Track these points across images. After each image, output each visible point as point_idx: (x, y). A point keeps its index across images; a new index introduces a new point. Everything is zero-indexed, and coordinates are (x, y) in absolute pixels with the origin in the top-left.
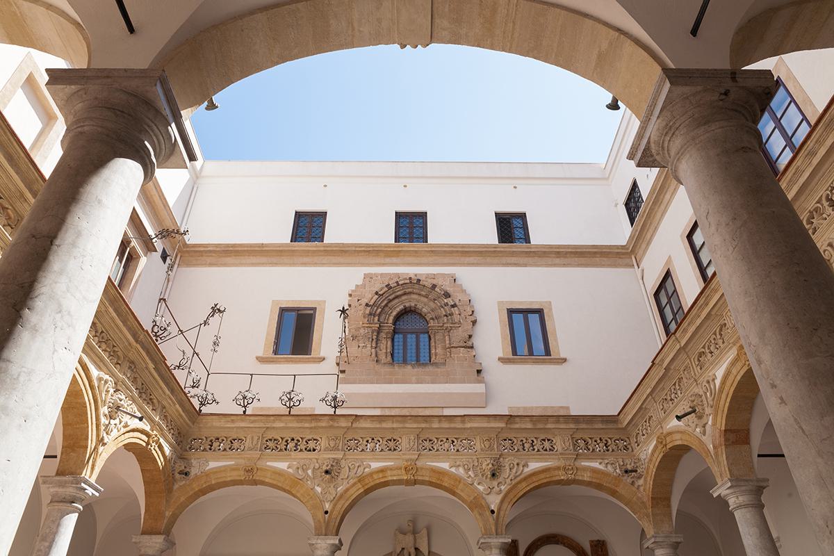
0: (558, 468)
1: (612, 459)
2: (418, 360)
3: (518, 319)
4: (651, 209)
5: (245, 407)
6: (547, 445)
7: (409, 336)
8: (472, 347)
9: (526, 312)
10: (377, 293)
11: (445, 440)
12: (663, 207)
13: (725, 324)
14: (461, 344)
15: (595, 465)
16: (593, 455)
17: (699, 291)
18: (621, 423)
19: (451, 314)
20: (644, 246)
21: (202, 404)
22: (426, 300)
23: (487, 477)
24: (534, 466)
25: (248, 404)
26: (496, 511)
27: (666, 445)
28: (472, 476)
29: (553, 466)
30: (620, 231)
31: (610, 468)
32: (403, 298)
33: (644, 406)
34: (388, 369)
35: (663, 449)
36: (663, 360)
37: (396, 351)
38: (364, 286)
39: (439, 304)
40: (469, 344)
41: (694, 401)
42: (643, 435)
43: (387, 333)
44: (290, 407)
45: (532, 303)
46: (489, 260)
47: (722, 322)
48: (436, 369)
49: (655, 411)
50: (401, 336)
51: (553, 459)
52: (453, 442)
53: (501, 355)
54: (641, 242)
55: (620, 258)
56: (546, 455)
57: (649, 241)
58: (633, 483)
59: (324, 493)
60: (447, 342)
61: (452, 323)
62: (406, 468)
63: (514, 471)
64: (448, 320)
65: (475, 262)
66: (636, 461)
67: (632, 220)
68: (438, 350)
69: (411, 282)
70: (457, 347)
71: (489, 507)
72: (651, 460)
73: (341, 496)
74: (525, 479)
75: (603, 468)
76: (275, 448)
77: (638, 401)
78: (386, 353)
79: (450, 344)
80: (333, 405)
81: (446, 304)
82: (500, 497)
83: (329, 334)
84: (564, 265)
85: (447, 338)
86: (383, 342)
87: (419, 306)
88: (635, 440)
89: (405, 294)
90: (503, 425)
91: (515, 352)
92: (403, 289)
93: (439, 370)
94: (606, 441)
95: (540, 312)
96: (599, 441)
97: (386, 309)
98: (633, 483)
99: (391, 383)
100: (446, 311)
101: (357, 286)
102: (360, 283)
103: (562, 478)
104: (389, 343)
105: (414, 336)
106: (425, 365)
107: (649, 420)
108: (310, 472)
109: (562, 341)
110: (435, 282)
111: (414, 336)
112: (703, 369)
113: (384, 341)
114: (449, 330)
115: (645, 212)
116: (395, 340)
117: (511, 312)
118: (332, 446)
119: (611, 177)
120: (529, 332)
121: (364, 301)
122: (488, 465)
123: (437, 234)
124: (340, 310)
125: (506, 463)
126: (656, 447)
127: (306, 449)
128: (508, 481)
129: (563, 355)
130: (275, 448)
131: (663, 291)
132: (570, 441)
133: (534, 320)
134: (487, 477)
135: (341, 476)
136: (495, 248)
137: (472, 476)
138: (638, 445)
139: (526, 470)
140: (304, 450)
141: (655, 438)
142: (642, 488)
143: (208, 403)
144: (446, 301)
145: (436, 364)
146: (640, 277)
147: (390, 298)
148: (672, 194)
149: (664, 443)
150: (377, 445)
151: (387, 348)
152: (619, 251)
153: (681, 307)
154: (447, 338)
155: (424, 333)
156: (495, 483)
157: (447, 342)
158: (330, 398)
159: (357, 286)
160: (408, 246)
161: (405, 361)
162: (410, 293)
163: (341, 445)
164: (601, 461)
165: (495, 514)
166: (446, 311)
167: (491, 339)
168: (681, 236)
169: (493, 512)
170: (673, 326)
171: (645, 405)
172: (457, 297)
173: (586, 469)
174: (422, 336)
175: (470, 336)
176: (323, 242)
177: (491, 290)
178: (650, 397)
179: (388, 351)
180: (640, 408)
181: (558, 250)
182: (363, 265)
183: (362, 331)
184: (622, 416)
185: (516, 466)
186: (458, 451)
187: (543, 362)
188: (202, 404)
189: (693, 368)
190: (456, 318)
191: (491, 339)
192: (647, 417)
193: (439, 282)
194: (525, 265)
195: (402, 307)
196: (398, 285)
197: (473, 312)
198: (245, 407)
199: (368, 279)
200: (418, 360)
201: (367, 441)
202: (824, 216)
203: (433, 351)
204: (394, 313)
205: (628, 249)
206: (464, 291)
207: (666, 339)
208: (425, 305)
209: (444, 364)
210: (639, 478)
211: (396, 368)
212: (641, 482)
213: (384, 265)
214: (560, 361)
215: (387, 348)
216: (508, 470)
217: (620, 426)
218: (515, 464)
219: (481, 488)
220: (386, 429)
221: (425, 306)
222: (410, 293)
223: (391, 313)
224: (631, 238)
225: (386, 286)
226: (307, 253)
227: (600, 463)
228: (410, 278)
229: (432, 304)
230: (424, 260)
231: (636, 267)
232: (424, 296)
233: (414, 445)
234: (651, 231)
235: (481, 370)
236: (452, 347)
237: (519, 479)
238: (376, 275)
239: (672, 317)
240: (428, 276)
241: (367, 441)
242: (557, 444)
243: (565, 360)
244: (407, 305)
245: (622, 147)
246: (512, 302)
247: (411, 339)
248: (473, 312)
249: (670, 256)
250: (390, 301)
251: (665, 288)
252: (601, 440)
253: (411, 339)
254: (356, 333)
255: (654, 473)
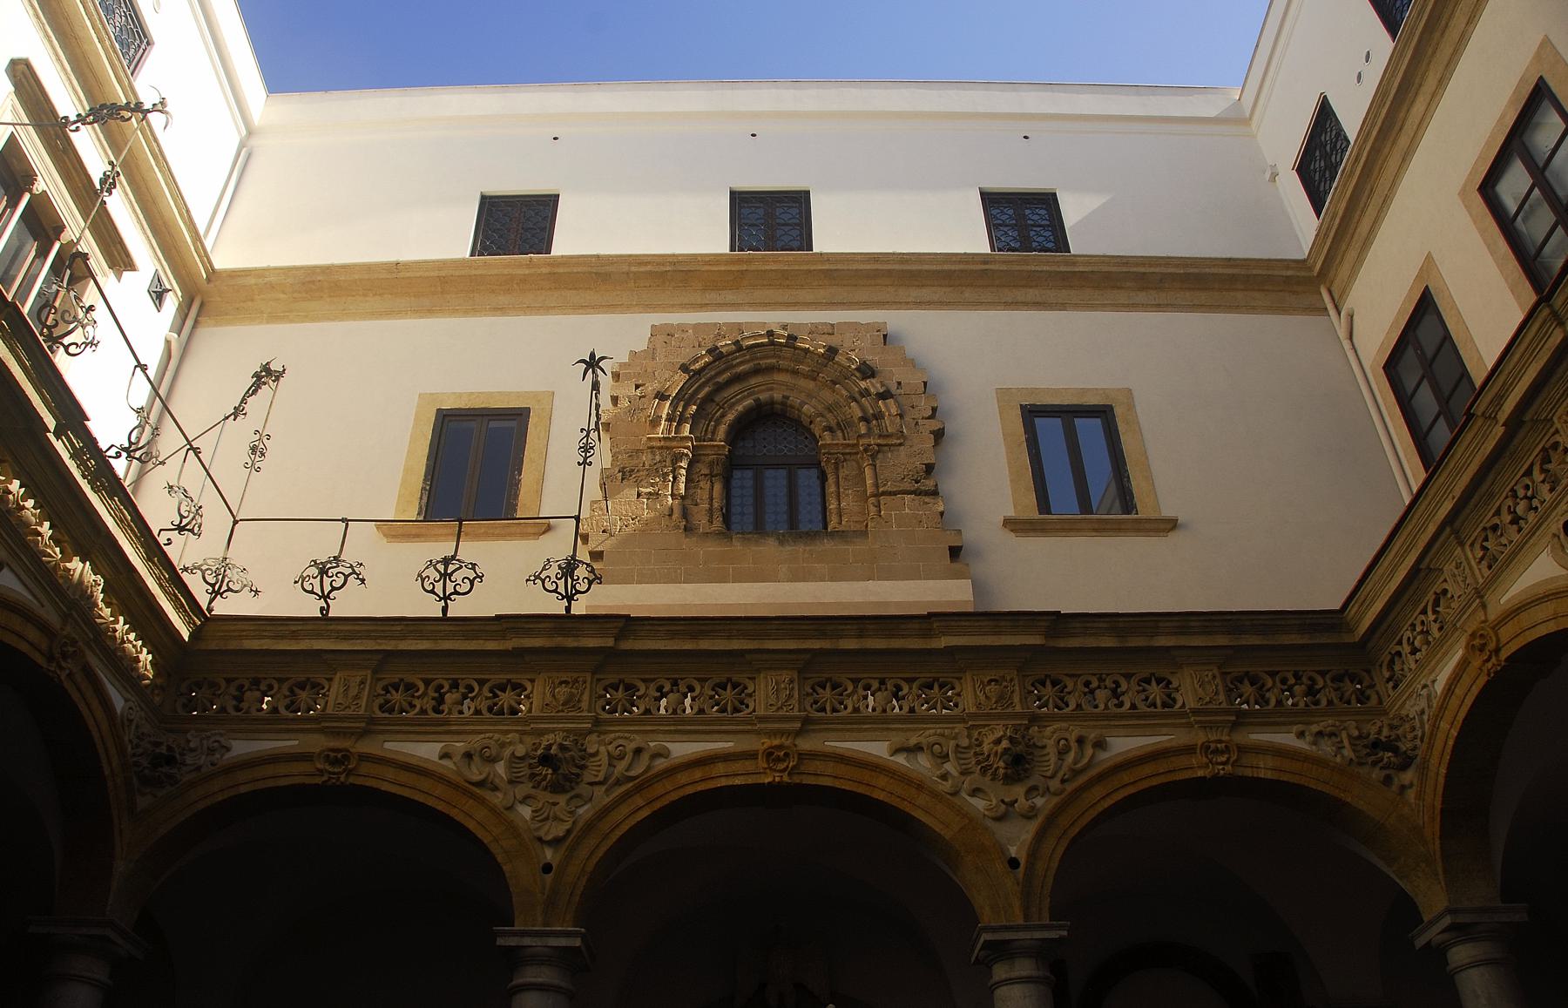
0: (1189, 750)
1: (1327, 723)
2: (793, 523)
3: (1050, 429)
4: (1376, 151)
5: (325, 597)
6: (1155, 691)
7: (769, 473)
8: (934, 493)
9: (1068, 413)
10: (684, 368)
11: (875, 685)
12: (1403, 141)
13: (1445, 591)
14: (906, 486)
15: (1286, 738)
16: (1277, 718)
17: (1519, 317)
18: (1351, 631)
19: (878, 416)
20: (1352, 255)
21: (216, 593)
22: (811, 385)
23: (995, 774)
24: (1124, 744)
25: (334, 589)
26: (1023, 862)
27: (1497, 651)
28: (954, 772)
29: (1174, 744)
30: (1298, 226)
31: (1326, 748)
32: (753, 381)
33: (1423, 566)
34: (713, 547)
35: (1489, 665)
36: (1499, 399)
37: (735, 510)
38: (651, 352)
39: (845, 393)
40: (929, 484)
41: (1396, 728)
42: (1414, 651)
43: (711, 465)
44: (446, 598)
45: (1084, 391)
46: (968, 294)
47: (1438, 587)
48: (843, 547)
49: (1459, 570)
50: (749, 474)
51: (1174, 725)
52: (899, 688)
53: (1011, 513)
54: (1344, 247)
55: (1294, 293)
56: (1154, 716)
57: (1367, 238)
58: (1387, 780)
59: (541, 817)
60: (869, 482)
61: (880, 436)
62: (771, 754)
63: (1070, 757)
64: (869, 429)
65: (936, 298)
66: (1395, 722)
67: (1317, 206)
68: (845, 504)
69: (772, 343)
70: (895, 494)
71: (1003, 851)
72: (1443, 708)
73: (590, 826)
74: (1101, 777)
75: (1307, 747)
76: (405, 705)
77: (1408, 551)
78: (711, 510)
79: (877, 486)
80: (562, 590)
81: (865, 393)
82: (1032, 827)
83: (559, 477)
84: (1159, 307)
85: (868, 472)
86: (702, 484)
87: (795, 400)
88: (1387, 675)
89: (757, 371)
90: (1036, 640)
91: (1044, 505)
92: (752, 360)
93: (850, 548)
94: (1311, 679)
95: (1104, 413)
96: (1292, 681)
97: (711, 408)
98: (1387, 780)
99: (723, 580)
100: (863, 409)
101: (633, 354)
102: (641, 345)
103: (1200, 773)
104: (718, 487)
105: (783, 473)
106: (811, 536)
107: (1436, 603)
108: (500, 768)
109: (1164, 478)
110: (834, 341)
111: (783, 473)
112: (1402, 686)
113: (704, 484)
114: (874, 454)
115: (1357, 159)
116: (734, 483)
117: (1032, 413)
118: (562, 699)
119: (1255, 118)
120: (1080, 458)
121: (651, 387)
122: (998, 742)
123: (837, 231)
124: (583, 361)
125: (1048, 737)
126: (1463, 664)
127: (490, 710)
128: (1055, 784)
129: (1167, 512)
130: (405, 705)
131: (1410, 353)
132: (1218, 680)
133: (1090, 430)
134: (995, 774)
135: (588, 776)
136: (985, 263)
137: (954, 772)
138: (1395, 687)
139: (1103, 756)
140: (484, 711)
141: (1463, 640)
142: (1411, 794)
143: (229, 590)
144: (863, 384)
145: (841, 535)
146: (1342, 333)
147: (720, 379)
148: (1404, 160)
149: (1492, 646)
150: (688, 701)
151: (711, 499)
152: (1289, 273)
153: (1465, 374)
154: (868, 472)
155: (809, 466)
156: (1019, 791)
157: (869, 482)
158: (554, 571)
159: (633, 354)
160: (764, 260)
161: (759, 529)
162: (770, 369)
163: (586, 697)
164: (1300, 727)
165: (1021, 869)
166: (863, 409)
167: (987, 477)
168: (1463, 193)
169: (1014, 863)
170: (1441, 435)
171: (1427, 560)
172: (894, 375)
173: (1259, 750)
174: (802, 473)
175: (929, 469)
176: (545, 245)
177: (984, 362)
178: (1448, 530)
179: (716, 505)
180: (1415, 571)
181: (1142, 270)
182: (649, 307)
183: (646, 458)
184: (1353, 609)
185: (1074, 745)
186: (912, 710)
187: (1117, 529)
188: (216, 593)
189: (1471, 568)
190: (890, 425)
191: (987, 477)
192: (1430, 597)
193: (844, 341)
194: (1062, 307)
195: (749, 402)
196: (740, 349)
197: (934, 410)
198: (325, 597)
199: (661, 338)
200: (793, 523)
201: (660, 689)
202: (1504, 541)
203: (832, 506)
204: (730, 417)
205: (1310, 269)
206: (912, 363)
207: (1423, 475)
208: (810, 396)
209: (864, 533)
210: (1404, 767)
211: (737, 545)
212: (1408, 776)
213: (703, 307)
214: (1162, 526)
215: (711, 499)
216: (1053, 758)
217: (1347, 639)
218: (1073, 738)
219: (979, 804)
220: (708, 656)
221: (808, 400)
222: (770, 369)
223: (723, 416)
224: (1320, 236)
225: (709, 352)
226: (508, 284)
227: (1301, 735)
228: (770, 333)
229: (827, 395)
230: (805, 295)
231: (1332, 312)
232: (806, 376)
233: (790, 696)
234: (1371, 212)
235: (960, 548)
236: (884, 493)
237: (1082, 779)
238: (683, 328)
239: (1436, 409)
240: (814, 330)
241: (660, 689)
242: (1182, 690)
243: (1170, 525)
244: (763, 397)
245: (1261, 102)
246: (1033, 391)
247: (775, 481)
248: (934, 410)
249: (1429, 257)
250: (720, 388)
251: (1424, 334)
252: (1297, 676)
253: (775, 481)
254: (629, 464)
255: (1451, 743)
